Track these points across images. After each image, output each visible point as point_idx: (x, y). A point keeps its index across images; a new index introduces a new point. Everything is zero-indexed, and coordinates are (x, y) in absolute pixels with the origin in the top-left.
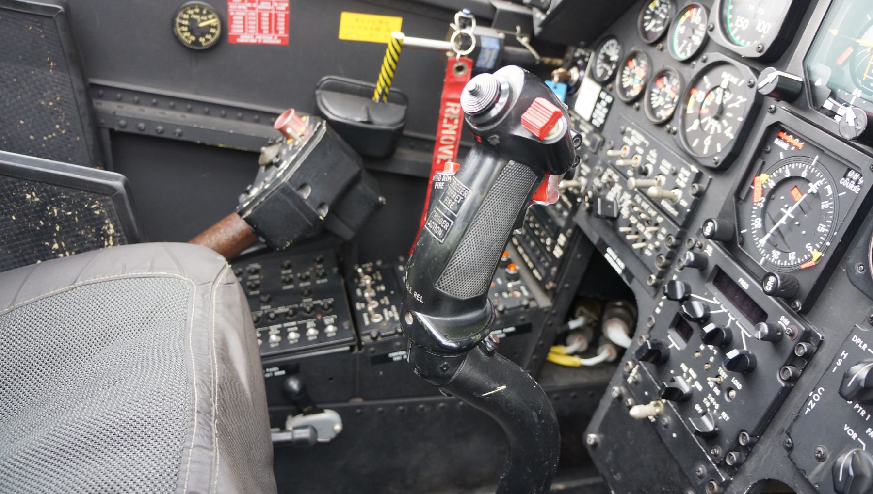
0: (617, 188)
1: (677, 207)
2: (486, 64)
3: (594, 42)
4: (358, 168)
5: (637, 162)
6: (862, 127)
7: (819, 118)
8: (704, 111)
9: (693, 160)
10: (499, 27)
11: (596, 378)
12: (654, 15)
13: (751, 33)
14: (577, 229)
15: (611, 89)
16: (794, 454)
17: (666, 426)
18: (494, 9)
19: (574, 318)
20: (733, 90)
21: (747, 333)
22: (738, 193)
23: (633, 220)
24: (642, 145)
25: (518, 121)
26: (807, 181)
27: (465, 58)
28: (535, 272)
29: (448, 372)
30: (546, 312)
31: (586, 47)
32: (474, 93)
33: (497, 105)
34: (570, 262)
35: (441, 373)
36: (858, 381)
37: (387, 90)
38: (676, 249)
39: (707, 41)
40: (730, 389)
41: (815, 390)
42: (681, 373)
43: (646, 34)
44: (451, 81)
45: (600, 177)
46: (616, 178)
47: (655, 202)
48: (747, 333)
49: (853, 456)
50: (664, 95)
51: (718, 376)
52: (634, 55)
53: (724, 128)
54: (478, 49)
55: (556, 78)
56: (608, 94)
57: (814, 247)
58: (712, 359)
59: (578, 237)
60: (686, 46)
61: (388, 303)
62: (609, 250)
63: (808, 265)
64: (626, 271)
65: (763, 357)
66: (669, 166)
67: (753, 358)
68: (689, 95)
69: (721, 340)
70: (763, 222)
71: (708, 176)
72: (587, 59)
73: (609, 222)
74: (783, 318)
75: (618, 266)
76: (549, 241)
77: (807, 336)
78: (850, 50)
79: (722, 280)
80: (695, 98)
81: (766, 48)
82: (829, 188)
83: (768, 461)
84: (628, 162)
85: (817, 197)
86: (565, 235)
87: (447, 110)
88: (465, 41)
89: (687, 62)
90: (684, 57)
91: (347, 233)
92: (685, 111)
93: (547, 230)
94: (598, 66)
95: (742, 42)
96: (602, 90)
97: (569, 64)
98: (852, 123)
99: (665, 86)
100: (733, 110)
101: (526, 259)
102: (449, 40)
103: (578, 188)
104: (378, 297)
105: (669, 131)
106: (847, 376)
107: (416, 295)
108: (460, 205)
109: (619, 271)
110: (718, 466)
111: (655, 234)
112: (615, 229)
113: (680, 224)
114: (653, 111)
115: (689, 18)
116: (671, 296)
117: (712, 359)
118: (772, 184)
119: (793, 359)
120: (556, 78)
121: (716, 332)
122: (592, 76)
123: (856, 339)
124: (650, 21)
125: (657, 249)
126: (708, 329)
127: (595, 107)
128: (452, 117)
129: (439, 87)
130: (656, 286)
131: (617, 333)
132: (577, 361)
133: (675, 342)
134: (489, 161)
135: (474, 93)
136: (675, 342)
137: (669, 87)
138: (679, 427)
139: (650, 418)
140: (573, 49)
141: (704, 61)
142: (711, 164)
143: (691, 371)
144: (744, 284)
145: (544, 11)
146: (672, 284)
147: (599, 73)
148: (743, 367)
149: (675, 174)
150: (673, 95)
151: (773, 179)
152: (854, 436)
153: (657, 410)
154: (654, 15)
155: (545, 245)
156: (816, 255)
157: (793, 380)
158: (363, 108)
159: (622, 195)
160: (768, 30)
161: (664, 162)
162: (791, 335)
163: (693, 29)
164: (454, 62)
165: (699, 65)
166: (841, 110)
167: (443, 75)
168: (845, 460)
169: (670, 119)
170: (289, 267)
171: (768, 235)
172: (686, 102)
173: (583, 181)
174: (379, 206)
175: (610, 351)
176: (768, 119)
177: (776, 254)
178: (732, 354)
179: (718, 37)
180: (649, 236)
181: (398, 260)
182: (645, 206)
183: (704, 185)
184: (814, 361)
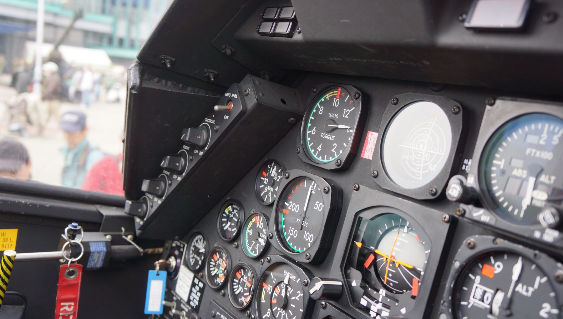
2: (95, 264)
3: (187, 236)
8: (274, 301)
10: (106, 231)
12: (229, 219)
18: (102, 215)
27: (76, 264)
31: (181, 239)
39: (268, 246)
43: (224, 233)
44: (64, 284)
54: (88, 254)
55: (158, 268)
60: (255, 245)
68: (262, 288)
72: (182, 250)
78: (372, 257)
80: (265, 290)
81: (312, 257)
87: (62, 309)
88: (74, 249)
89: (257, 259)
94: (191, 256)
96: (195, 277)
99: (242, 277)
114: (236, 297)
115: (254, 224)
120: (158, 268)
122: (187, 265)
124: (226, 222)
127: (191, 291)
128: (66, 314)
137: (245, 278)
140: (170, 242)
141: (269, 262)
145: (142, 218)
154: (229, 219)
163: (258, 234)
164: (66, 268)
179: (275, 242)
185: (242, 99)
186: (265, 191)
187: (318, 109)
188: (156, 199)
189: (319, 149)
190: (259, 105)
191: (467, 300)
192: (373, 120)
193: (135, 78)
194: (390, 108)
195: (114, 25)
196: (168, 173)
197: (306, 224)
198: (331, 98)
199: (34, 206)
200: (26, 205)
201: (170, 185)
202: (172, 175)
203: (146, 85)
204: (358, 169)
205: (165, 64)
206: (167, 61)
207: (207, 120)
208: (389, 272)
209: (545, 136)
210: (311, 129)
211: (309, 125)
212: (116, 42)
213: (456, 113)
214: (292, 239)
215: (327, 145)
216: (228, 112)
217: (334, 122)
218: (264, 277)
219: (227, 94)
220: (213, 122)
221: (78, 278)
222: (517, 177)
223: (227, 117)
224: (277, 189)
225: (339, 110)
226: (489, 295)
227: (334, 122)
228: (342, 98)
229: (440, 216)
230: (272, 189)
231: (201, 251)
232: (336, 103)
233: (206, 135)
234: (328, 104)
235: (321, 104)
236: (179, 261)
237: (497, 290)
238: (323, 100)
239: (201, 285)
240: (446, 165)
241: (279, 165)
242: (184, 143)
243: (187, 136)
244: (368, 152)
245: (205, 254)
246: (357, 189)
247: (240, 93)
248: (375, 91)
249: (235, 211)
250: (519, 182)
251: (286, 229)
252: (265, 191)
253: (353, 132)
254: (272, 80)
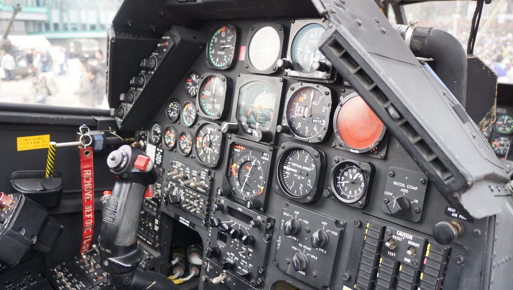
0: (176, 189)
1: (204, 188)
3: (148, 127)
4: (46, 214)
5: (181, 175)
6: (261, 136)
7: (248, 137)
8: (204, 145)
9: (205, 166)
11: (193, 285)
13: (213, 110)
14: (163, 214)
15: (161, 146)
16: (280, 267)
17: (230, 282)
18: (97, 121)
19: (173, 260)
20: (213, 134)
21: (247, 228)
22: (227, 174)
23: (187, 200)
24: (182, 167)
25: (132, 165)
26: (250, 161)
28: (148, 242)
29: (129, 282)
30: (159, 259)
32: (113, 159)
33: (123, 162)
34: (164, 230)
35: (126, 283)
36: (289, 227)
37: (52, 171)
38: (209, 206)
39: (197, 116)
40: (249, 254)
41: (278, 239)
42: (228, 256)
43: (171, 118)
44: (84, 159)
45: (167, 186)
46: (174, 184)
47: (194, 189)
48: (247, 228)
49: (297, 255)
50: (186, 143)
51: (243, 250)
52: (167, 129)
53: (214, 150)
54: (94, 141)
56: (160, 149)
57: (260, 186)
58: (238, 245)
59: (164, 217)
60: (189, 120)
61: (76, 281)
62: (181, 218)
63: (260, 193)
64: (191, 224)
65: (257, 235)
66: (196, 172)
67: (253, 237)
68: (196, 140)
69: (238, 235)
70: (240, 183)
71: (213, 172)
73: (177, 205)
74: (258, 217)
75: (187, 223)
76: (150, 225)
77: (269, 220)
79: (232, 212)
82: (258, 161)
83: (273, 275)
84: (178, 176)
85: (256, 166)
86: (157, 219)
87: (85, 174)
88: (86, 139)
89: (192, 126)
90: (189, 125)
91: (47, 249)
92: (196, 147)
93: (148, 220)
95: (211, 114)
96: (157, 147)
97: (138, 139)
98: (257, 136)
100: (215, 142)
101: (142, 237)
102: (78, 140)
103: (158, 195)
104: (70, 280)
105: (192, 158)
106: (285, 227)
107: (107, 251)
108: (117, 206)
109: (188, 225)
110: (255, 287)
111: (198, 203)
112: (180, 207)
113: (208, 195)
114: (183, 151)
115: (188, 108)
116: (213, 226)
117: (238, 245)
118: (238, 167)
119: (268, 231)
121: (235, 232)
122: (151, 142)
123: (285, 214)
124: (171, 112)
125: (201, 209)
126: (232, 232)
127: (156, 156)
128: (88, 177)
129: (79, 164)
130: (206, 225)
131: (196, 260)
132: (181, 280)
133: (221, 245)
134: (124, 185)
135: (113, 159)
136: (221, 245)
137: (186, 139)
138: (235, 280)
139: (222, 282)
140: (138, 131)
141: (198, 125)
142: (213, 166)
143: (232, 254)
144: (240, 210)
145: (121, 117)
146: (212, 221)
147: (154, 140)
148: (251, 242)
149: (199, 175)
150: (189, 142)
151: (238, 165)
152: (296, 249)
153: (224, 277)
155: (149, 227)
156: (262, 188)
157: (270, 239)
158: (39, 183)
159: (179, 191)
160: (219, 108)
161: (193, 171)
162: (263, 222)
164: (84, 150)
165: (197, 127)
166: (254, 132)
167: (79, 158)
168: (295, 258)
169: (191, 152)
170: (10, 283)
171: (243, 187)
172: (196, 144)
173: (159, 191)
174: (62, 230)
175: (195, 270)
176: (229, 142)
177: (248, 193)
178: (244, 238)
179: (201, 114)
180: (196, 205)
181: (74, 259)
182: (191, 192)
183: (213, 176)
184: (275, 228)
185: (169, 41)
186: (191, 89)
187: (214, 40)
188: (128, 105)
189: (217, 60)
190: (182, 41)
191: (293, 114)
192: (243, 40)
193: (112, 34)
194: (250, 33)
195: (48, 13)
196: (134, 89)
197: (215, 100)
198: (221, 33)
199: (58, 119)
200: (53, 119)
201: (136, 94)
202: (136, 89)
203: (118, 37)
204: (238, 66)
205: (128, 24)
206: (129, 23)
207: (153, 54)
208: (259, 114)
209: (316, 33)
210: (212, 50)
211: (211, 49)
212: (52, 27)
213: (281, 30)
214: (209, 110)
215: (221, 57)
216: (165, 47)
217: (223, 44)
218: (197, 134)
219: (163, 38)
220: (158, 54)
221: (91, 156)
222: (307, 54)
223: (165, 50)
224: (197, 87)
225: (225, 38)
226: (302, 110)
227: (223, 44)
228: (226, 32)
229: (278, 81)
230: (195, 87)
231: (158, 132)
232: (223, 35)
233: (154, 61)
234: (219, 37)
235: (216, 36)
236: (145, 142)
237: (306, 107)
238: (216, 34)
239: (161, 151)
240: (279, 55)
241: (197, 74)
242: (142, 68)
243: (144, 63)
244: (242, 57)
245: (161, 134)
246: (239, 76)
247: (171, 36)
248: (242, 25)
249: (175, 105)
250: (308, 56)
251: (205, 106)
252: (191, 89)
253: (233, 48)
254: (187, 27)
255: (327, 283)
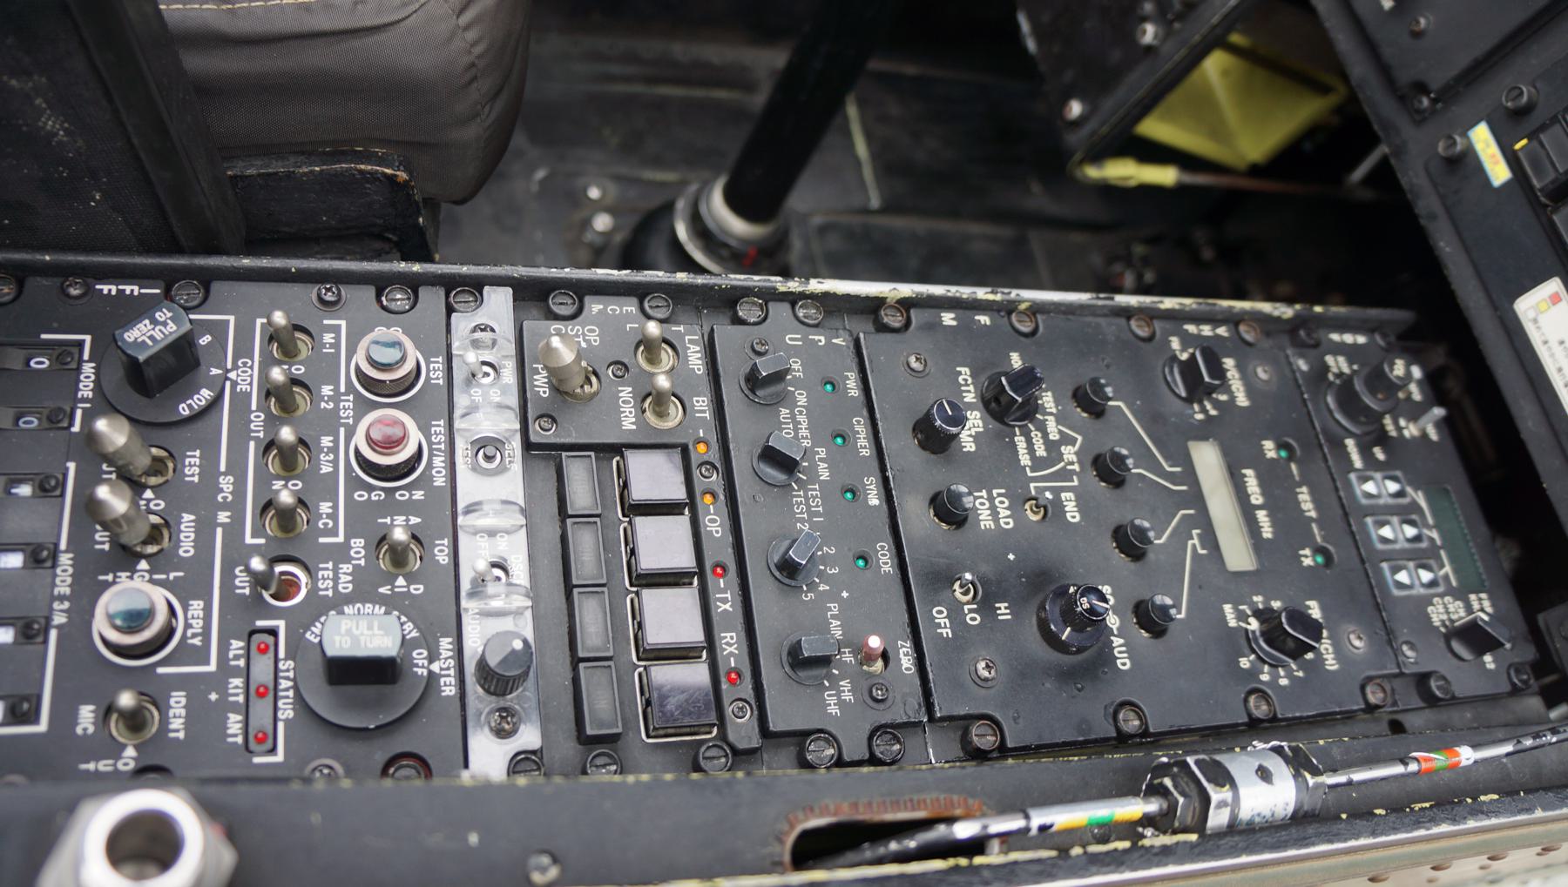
255: (1437, 80)
